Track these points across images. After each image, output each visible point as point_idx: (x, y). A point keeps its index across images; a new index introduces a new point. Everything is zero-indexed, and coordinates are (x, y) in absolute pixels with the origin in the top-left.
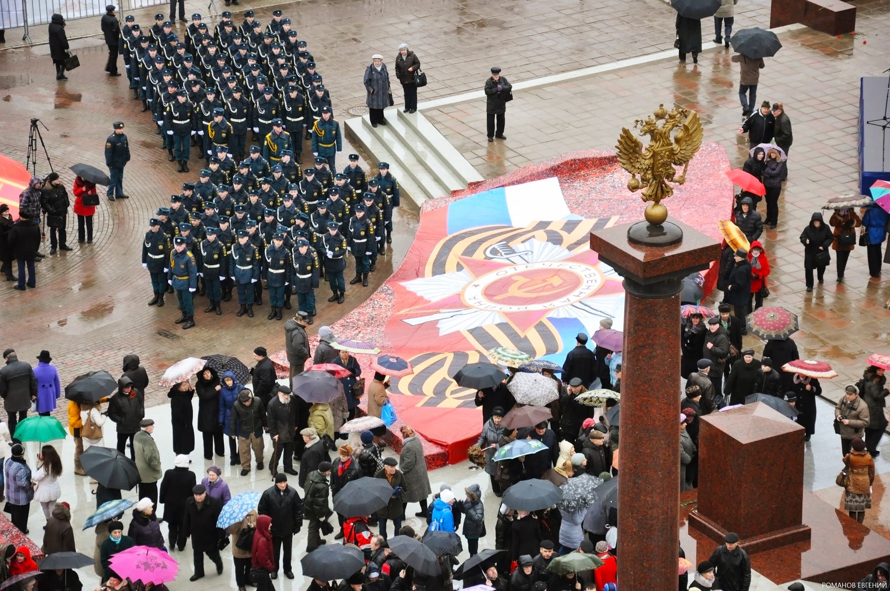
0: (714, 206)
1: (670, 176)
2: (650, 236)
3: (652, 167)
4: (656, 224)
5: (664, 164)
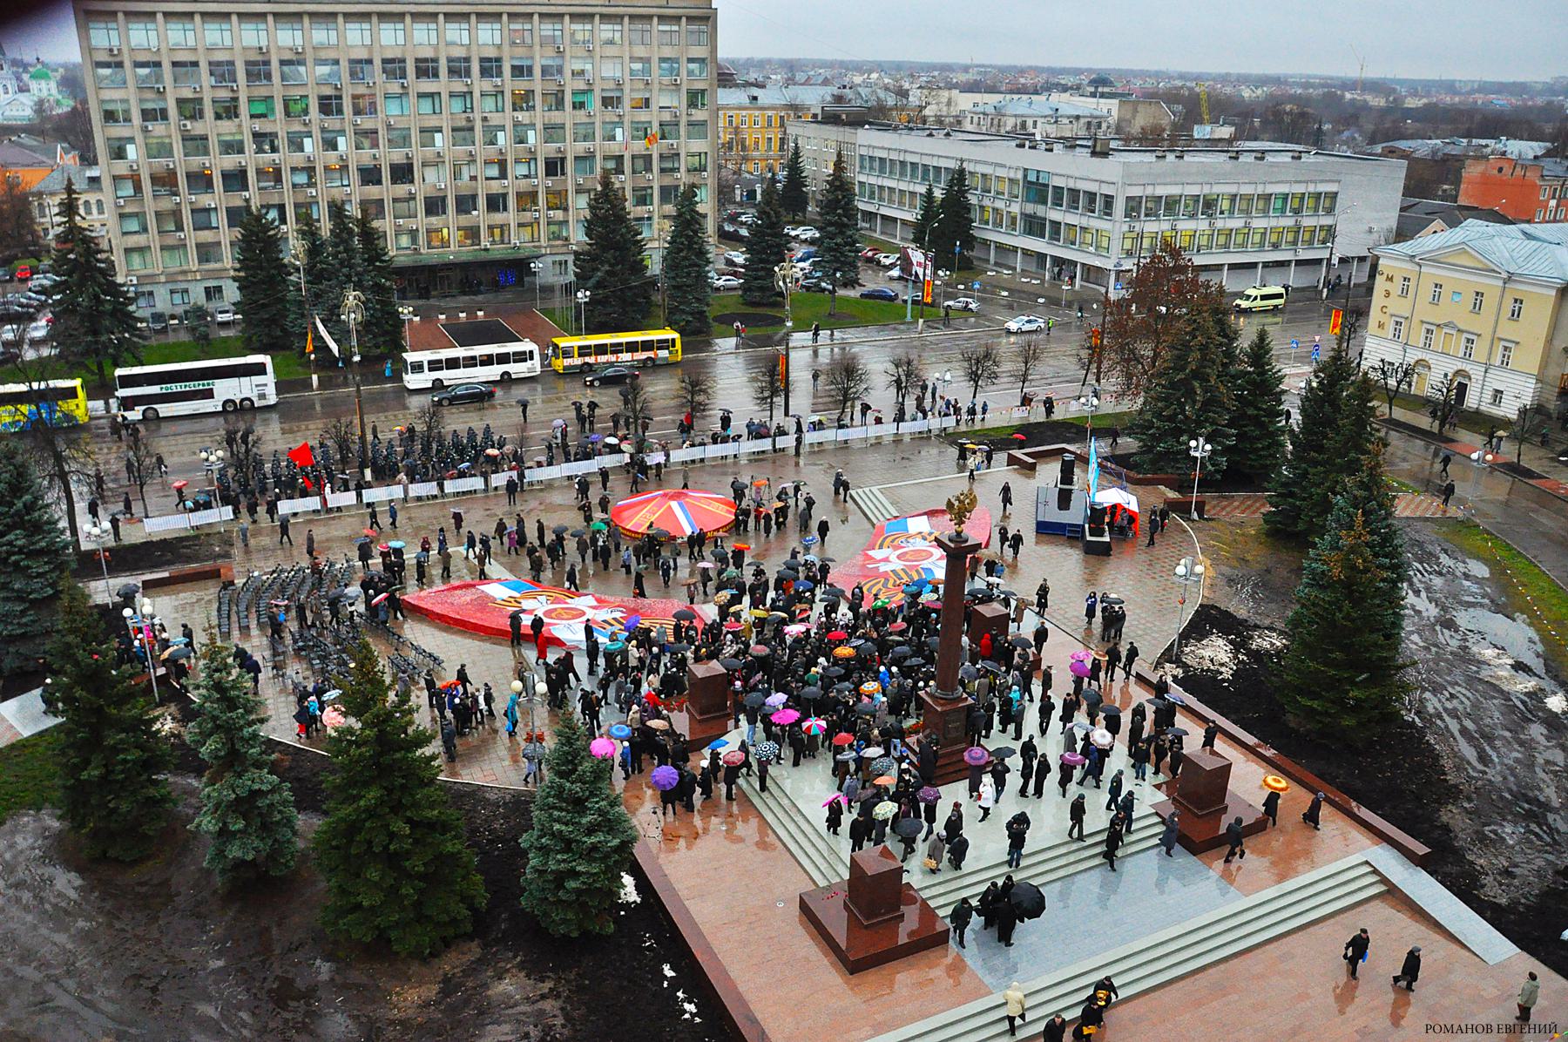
4: (959, 534)
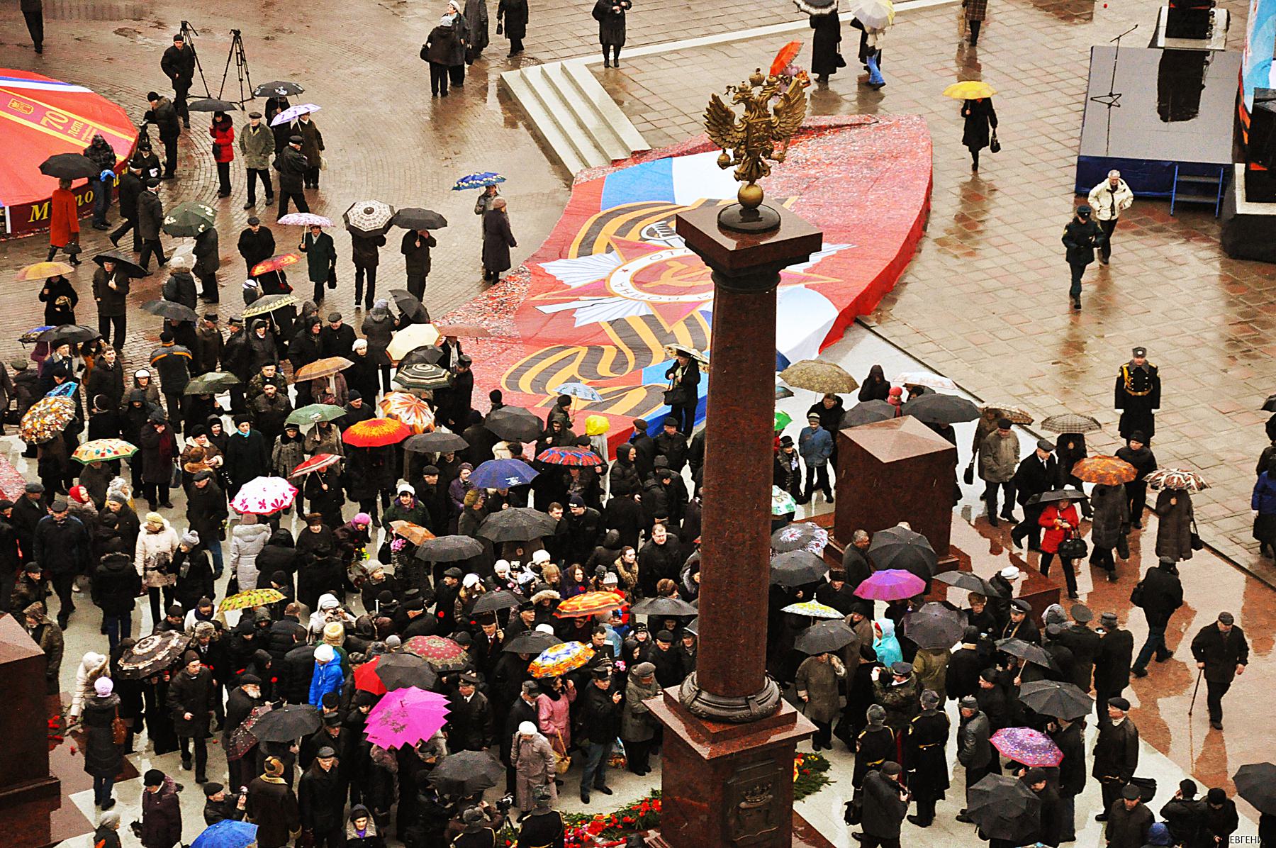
0: (907, 189)
1: (768, 154)
2: (743, 221)
3: (745, 142)
4: (750, 207)
5: (759, 139)
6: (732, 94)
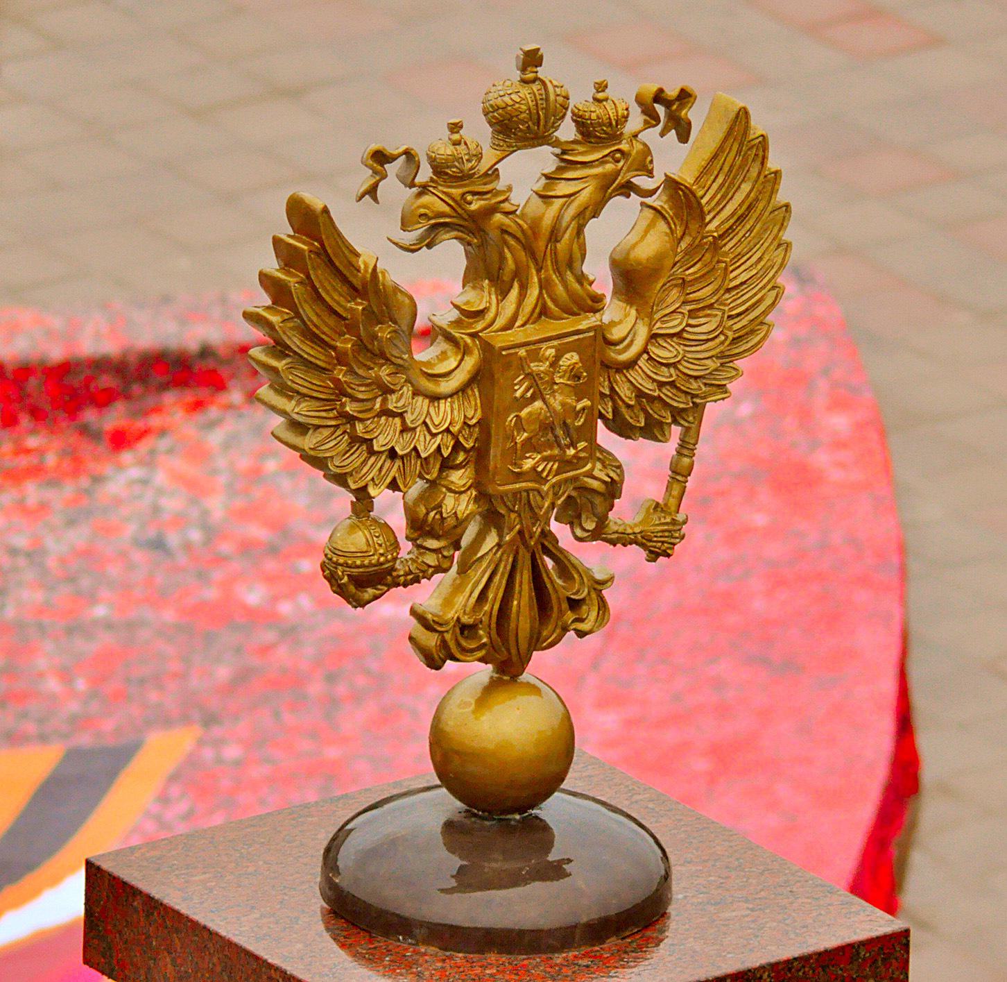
6: (394, 191)
